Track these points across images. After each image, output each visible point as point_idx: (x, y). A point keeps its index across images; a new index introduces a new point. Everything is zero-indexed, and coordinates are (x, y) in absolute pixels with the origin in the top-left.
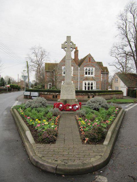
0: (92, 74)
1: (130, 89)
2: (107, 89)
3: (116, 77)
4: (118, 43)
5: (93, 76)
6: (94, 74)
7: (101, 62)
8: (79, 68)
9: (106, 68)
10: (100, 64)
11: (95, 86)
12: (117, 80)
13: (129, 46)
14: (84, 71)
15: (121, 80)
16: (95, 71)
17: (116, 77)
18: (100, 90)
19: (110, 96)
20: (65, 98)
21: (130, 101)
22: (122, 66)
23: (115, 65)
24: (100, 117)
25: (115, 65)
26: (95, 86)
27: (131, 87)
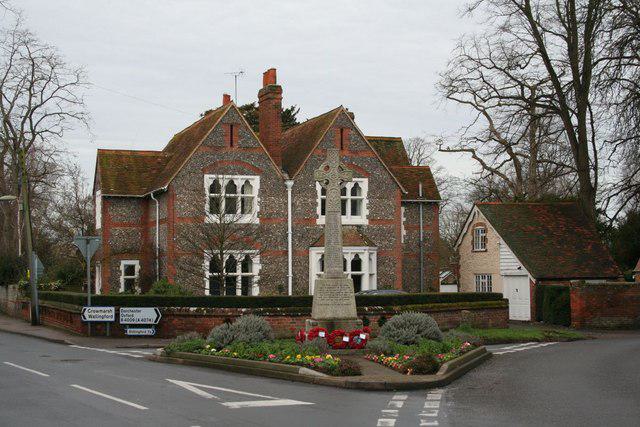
0: (354, 212)
1: (546, 283)
2: (432, 290)
3: (475, 222)
4: (484, 41)
5: (361, 219)
6: (365, 211)
7: (399, 140)
8: (290, 183)
9: (425, 174)
10: (390, 150)
11: (371, 275)
12: (485, 239)
13: (538, 59)
14: (316, 196)
15: (502, 241)
16: (369, 197)
17: (475, 222)
18: (397, 291)
19: (449, 315)
20: (329, 315)
21: (528, 335)
22: (513, 156)
23: (472, 151)
24: (459, 201)
25: (472, 151)
26: (375, 271)
27: (551, 274)
